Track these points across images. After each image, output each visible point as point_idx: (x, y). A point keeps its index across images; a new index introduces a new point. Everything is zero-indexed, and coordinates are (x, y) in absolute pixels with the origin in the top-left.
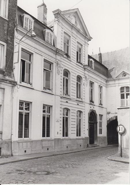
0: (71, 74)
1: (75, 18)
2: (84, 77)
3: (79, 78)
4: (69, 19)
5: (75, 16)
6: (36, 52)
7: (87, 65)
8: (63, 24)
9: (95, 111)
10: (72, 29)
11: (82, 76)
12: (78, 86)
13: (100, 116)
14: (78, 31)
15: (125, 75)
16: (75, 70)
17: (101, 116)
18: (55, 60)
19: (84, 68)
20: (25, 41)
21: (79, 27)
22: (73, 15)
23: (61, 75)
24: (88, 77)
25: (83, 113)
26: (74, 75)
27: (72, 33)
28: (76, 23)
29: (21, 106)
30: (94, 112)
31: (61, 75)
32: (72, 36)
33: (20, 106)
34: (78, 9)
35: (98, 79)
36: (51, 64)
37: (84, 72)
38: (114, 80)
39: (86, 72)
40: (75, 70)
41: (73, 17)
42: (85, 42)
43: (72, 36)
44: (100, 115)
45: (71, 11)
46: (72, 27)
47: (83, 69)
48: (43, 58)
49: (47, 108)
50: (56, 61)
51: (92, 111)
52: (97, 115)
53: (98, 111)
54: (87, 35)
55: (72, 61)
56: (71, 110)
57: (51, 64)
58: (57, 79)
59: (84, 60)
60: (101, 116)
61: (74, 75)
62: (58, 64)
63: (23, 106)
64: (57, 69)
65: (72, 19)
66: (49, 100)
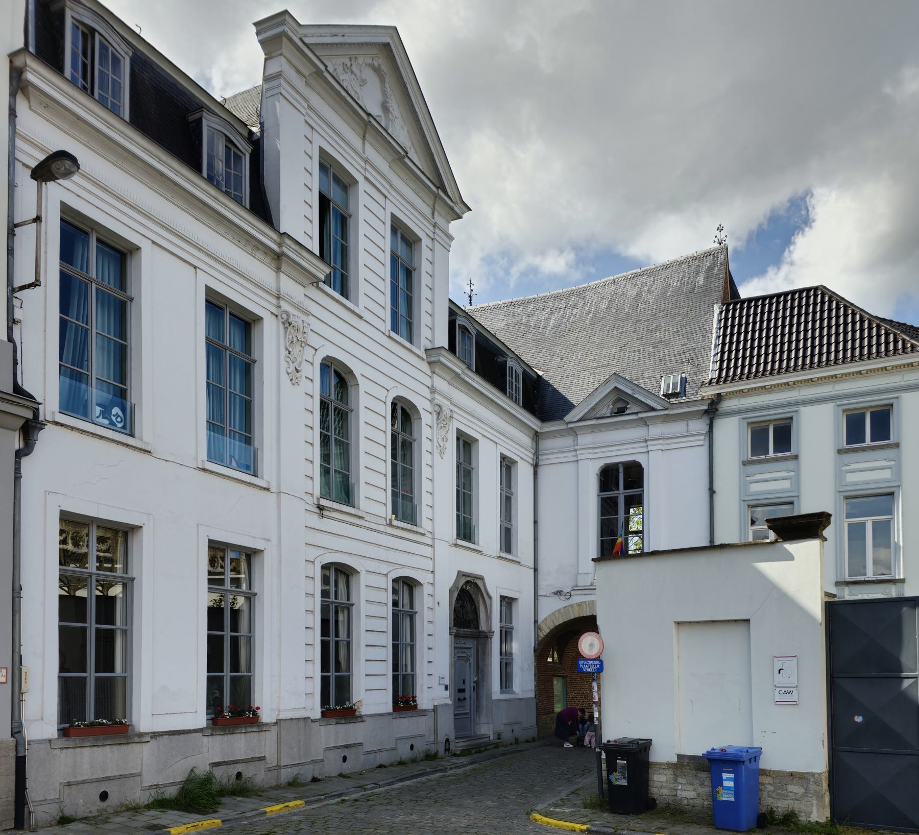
0: (364, 385)
1: (382, 79)
2: (429, 407)
3: (403, 414)
4: (345, 78)
5: (377, 70)
6: (153, 242)
7: (447, 348)
8: (317, 102)
9: (481, 578)
10: (364, 138)
11: (422, 404)
12: (403, 449)
13: (504, 603)
14: (399, 157)
15: (620, 405)
16: (387, 371)
17: (508, 602)
18: (274, 301)
19: (430, 363)
20: (18, 166)
21: (402, 134)
22: (369, 61)
23: (305, 385)
24: (446, 412)
25: (427, 589)
26: (381, 394)
27: (366, 161)
28: (385, 108)
29: (76, 544)
30: (476, 584)
31: (305, 385)
32: (366, 178)
33: (70, 547)
34: (395, 28)
35: (499, 430)
36: (246, 323)
37: (428, 382)
38: (574, 432)
39: (441, 384)
40: (387, 371)
41: (369, 75)
42: (433, 390)
43: (366, 178)
44: (503, 598)
45: (599, 390)
46: (367, 125)
47: (425, 367)
48: (204, 280)
49: (230, 564)
50: (279, 307)
51: (468, 582)
52: (490, 598)
53: (499, 579)
54: (442, 187)
55: (367, 316)
56: (363, 575)
57: (246, 323)
58: (288, 410)
59: (431, 587)
60: (508, 602)
61: (381, 394)
62: (288, 324)
63: (84, 550)
64: (284, 353)
65: (363, 82)
66: (236, 513)
